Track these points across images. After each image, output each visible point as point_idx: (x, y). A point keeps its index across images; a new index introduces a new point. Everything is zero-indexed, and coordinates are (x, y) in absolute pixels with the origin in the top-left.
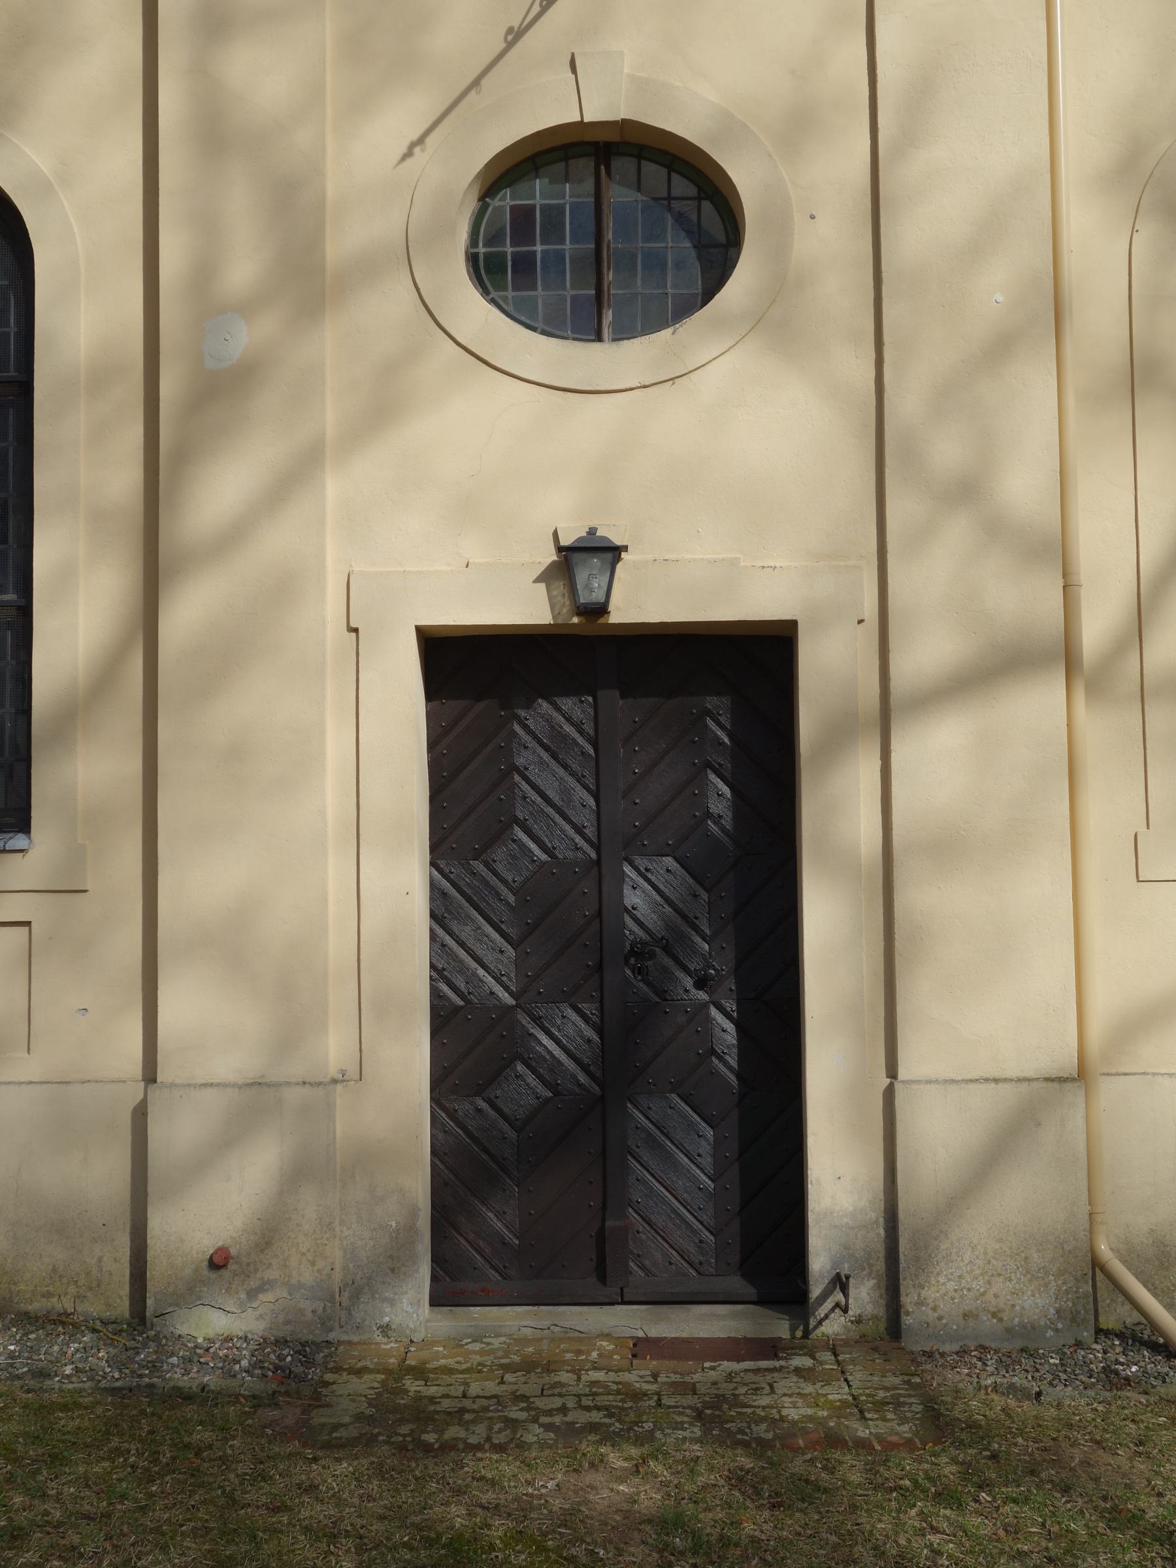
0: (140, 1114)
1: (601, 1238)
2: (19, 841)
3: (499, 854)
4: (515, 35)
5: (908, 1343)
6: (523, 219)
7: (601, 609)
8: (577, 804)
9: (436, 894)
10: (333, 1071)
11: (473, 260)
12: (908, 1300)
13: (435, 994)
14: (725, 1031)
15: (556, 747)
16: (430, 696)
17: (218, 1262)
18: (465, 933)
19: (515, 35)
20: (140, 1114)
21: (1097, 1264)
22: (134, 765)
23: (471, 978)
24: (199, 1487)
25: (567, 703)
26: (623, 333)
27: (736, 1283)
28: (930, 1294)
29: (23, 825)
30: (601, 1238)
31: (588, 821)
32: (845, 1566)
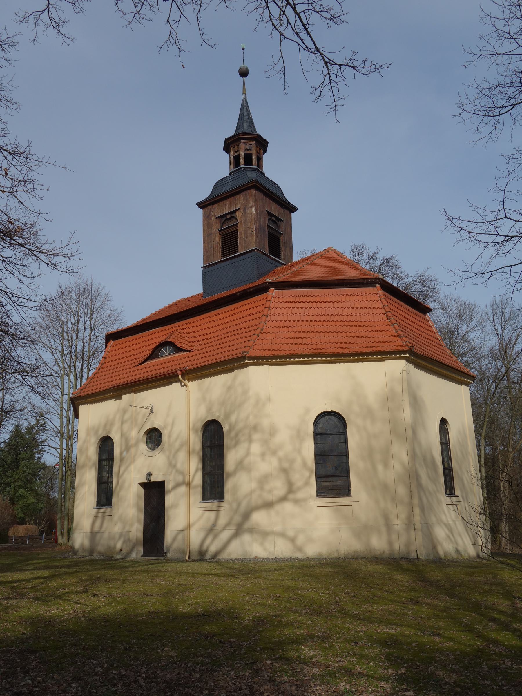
7: (150, 480)
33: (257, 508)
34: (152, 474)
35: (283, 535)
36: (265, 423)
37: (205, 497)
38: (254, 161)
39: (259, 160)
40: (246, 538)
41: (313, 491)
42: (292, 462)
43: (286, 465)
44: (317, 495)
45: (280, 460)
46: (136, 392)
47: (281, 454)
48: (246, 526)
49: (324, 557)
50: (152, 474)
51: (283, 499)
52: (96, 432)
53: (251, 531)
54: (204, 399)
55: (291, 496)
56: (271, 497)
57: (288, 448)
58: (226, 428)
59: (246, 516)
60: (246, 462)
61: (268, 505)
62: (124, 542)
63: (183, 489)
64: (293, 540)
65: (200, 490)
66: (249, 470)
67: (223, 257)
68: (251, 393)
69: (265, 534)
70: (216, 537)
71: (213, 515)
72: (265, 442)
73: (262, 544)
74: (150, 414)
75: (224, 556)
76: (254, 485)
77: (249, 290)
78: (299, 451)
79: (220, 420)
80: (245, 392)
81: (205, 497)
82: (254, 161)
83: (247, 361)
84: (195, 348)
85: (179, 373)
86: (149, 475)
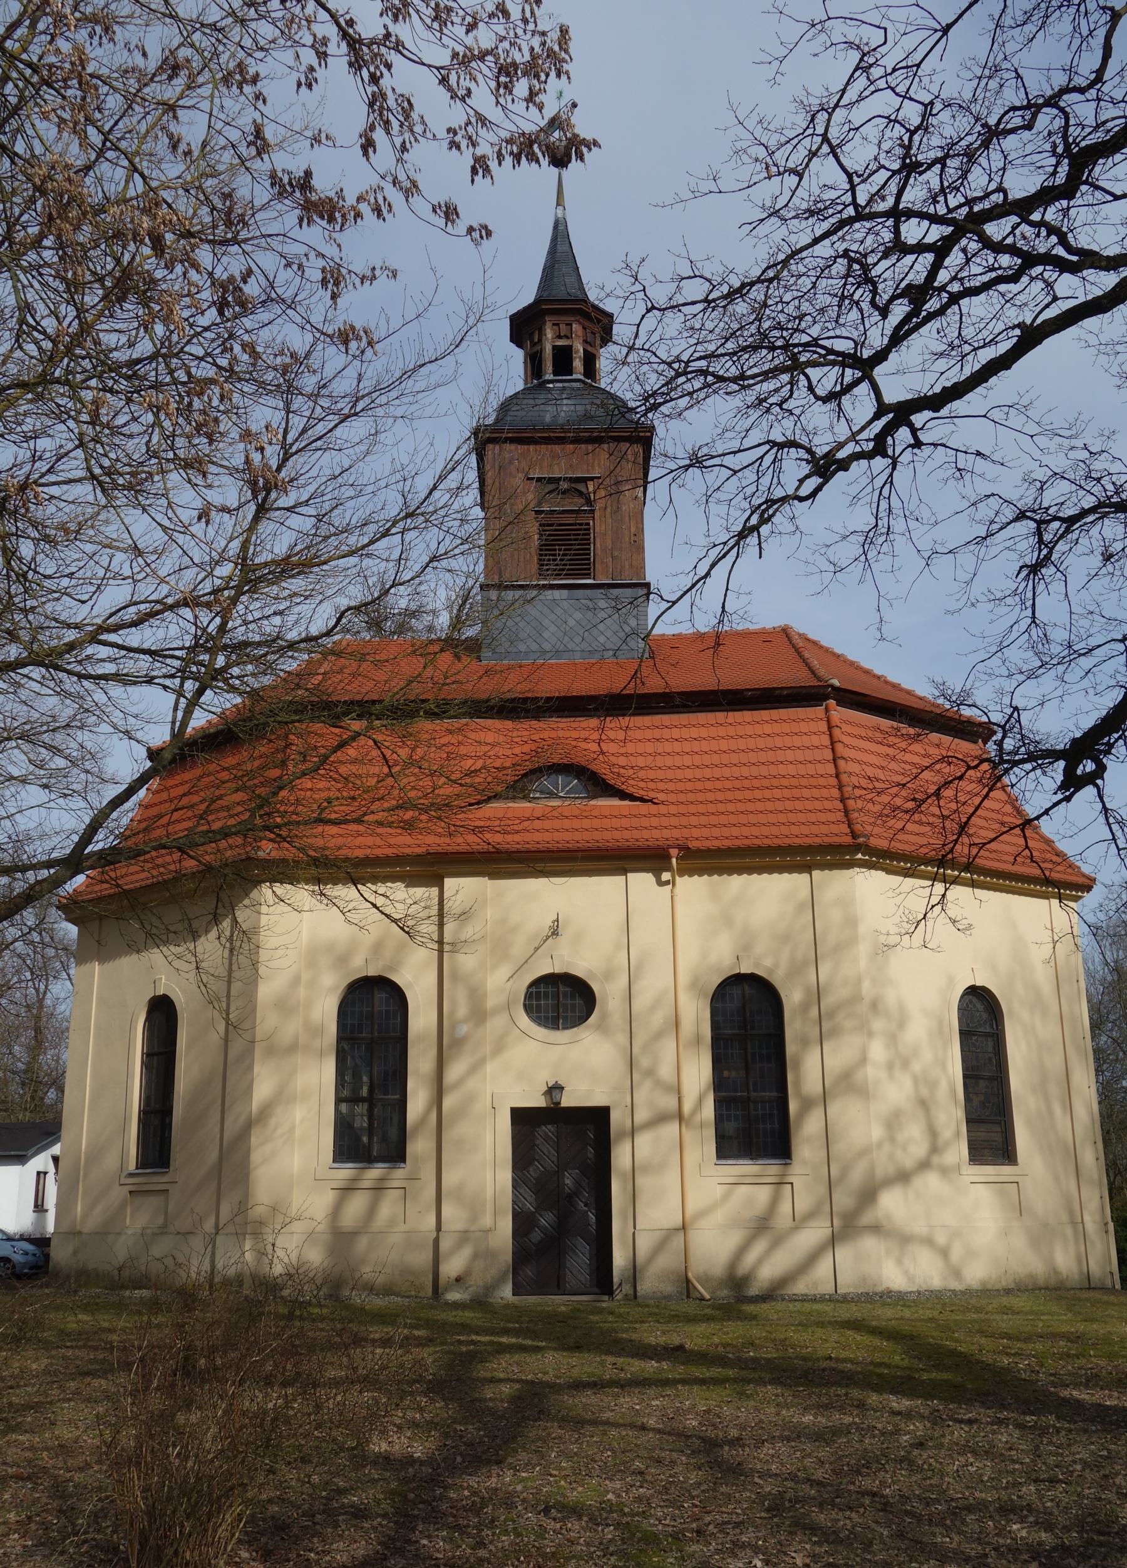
0: (436, 1241)
1: (558, 1277)
2: (402, 1165)
3: (531, 1169)
4: (536, 949)
5: (639, 1300)
6: (538, 994)
7: (559, 1103)
8: (67, 109)
9: (514, 1180)
10: (488, 1227)
11: (525, 1005)
12: (638, 1288)
13: (514, 1209)
14: (592, 1218)
15: (547, 1139)
16: (513, 1124)
17: (458, 1280)
18: (522, 1191)
19: (536, 949)
20: (436, 1241)
21: (688, 1281)
22: (433, 1144)
23: (523, 1204)
24: (262, 1535)
25: (549, 1127)
26: (565, 1028)
27: (596, 1290)
28: (644, 1287)
29: (404, 1161)
30: (558, 1277)
31: (555, 1160)
32: (680, 1566)
33: (889, 1182)
34: (563, 1088)
35: (929, 1241)
36: (891, 998)
37: (723, 1153)
38: (578, 364)
39: (590, 361)
40: (869, 1244)
41: (962, 1149)
42: (933, 1085)
43: (925, 1092)
44: (970, 1160)
45: (916, 1080)
46: (494, 875)
47: (916, 1067)
48: (867, 1219)
49: (1041, 1282)
50: (563, 1088)
51: (924, 1165)
52: (342, 960)
53: (876, 1229)
54: (727, 920)
55: (935, 1160)
56: (909, 1163)
57: (927, 1056)
58: (792, 997)
59: (868, 1195)
60: (859, 1076)
61: (903, 1177)
62: (475, 1256)
63: (671, 1130)
64: (944, 1253)
65: (710, 1133)
66: (863, 1092)
67: (541, 575)
68: (862, 929)
69: (904, 1240)
70: (777, 1242)
71: (763, 1194)
72: (892, 1039)
73: (899, 1262)
74: (548, 938)
75: (800, 1287)
76: (877, 1132)
77: (777, 692)
78: (944, 1068)
79: (777, 980)
80: (851, 922)
81: (723, 1153)
82: (578, 364)
83: (860, 856)
84: (661, 797)
85: (674, 852)
86: (555, 1090)
